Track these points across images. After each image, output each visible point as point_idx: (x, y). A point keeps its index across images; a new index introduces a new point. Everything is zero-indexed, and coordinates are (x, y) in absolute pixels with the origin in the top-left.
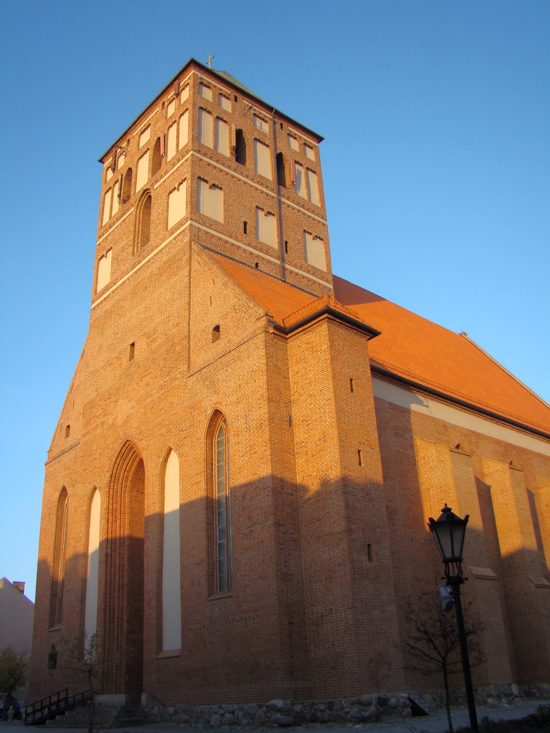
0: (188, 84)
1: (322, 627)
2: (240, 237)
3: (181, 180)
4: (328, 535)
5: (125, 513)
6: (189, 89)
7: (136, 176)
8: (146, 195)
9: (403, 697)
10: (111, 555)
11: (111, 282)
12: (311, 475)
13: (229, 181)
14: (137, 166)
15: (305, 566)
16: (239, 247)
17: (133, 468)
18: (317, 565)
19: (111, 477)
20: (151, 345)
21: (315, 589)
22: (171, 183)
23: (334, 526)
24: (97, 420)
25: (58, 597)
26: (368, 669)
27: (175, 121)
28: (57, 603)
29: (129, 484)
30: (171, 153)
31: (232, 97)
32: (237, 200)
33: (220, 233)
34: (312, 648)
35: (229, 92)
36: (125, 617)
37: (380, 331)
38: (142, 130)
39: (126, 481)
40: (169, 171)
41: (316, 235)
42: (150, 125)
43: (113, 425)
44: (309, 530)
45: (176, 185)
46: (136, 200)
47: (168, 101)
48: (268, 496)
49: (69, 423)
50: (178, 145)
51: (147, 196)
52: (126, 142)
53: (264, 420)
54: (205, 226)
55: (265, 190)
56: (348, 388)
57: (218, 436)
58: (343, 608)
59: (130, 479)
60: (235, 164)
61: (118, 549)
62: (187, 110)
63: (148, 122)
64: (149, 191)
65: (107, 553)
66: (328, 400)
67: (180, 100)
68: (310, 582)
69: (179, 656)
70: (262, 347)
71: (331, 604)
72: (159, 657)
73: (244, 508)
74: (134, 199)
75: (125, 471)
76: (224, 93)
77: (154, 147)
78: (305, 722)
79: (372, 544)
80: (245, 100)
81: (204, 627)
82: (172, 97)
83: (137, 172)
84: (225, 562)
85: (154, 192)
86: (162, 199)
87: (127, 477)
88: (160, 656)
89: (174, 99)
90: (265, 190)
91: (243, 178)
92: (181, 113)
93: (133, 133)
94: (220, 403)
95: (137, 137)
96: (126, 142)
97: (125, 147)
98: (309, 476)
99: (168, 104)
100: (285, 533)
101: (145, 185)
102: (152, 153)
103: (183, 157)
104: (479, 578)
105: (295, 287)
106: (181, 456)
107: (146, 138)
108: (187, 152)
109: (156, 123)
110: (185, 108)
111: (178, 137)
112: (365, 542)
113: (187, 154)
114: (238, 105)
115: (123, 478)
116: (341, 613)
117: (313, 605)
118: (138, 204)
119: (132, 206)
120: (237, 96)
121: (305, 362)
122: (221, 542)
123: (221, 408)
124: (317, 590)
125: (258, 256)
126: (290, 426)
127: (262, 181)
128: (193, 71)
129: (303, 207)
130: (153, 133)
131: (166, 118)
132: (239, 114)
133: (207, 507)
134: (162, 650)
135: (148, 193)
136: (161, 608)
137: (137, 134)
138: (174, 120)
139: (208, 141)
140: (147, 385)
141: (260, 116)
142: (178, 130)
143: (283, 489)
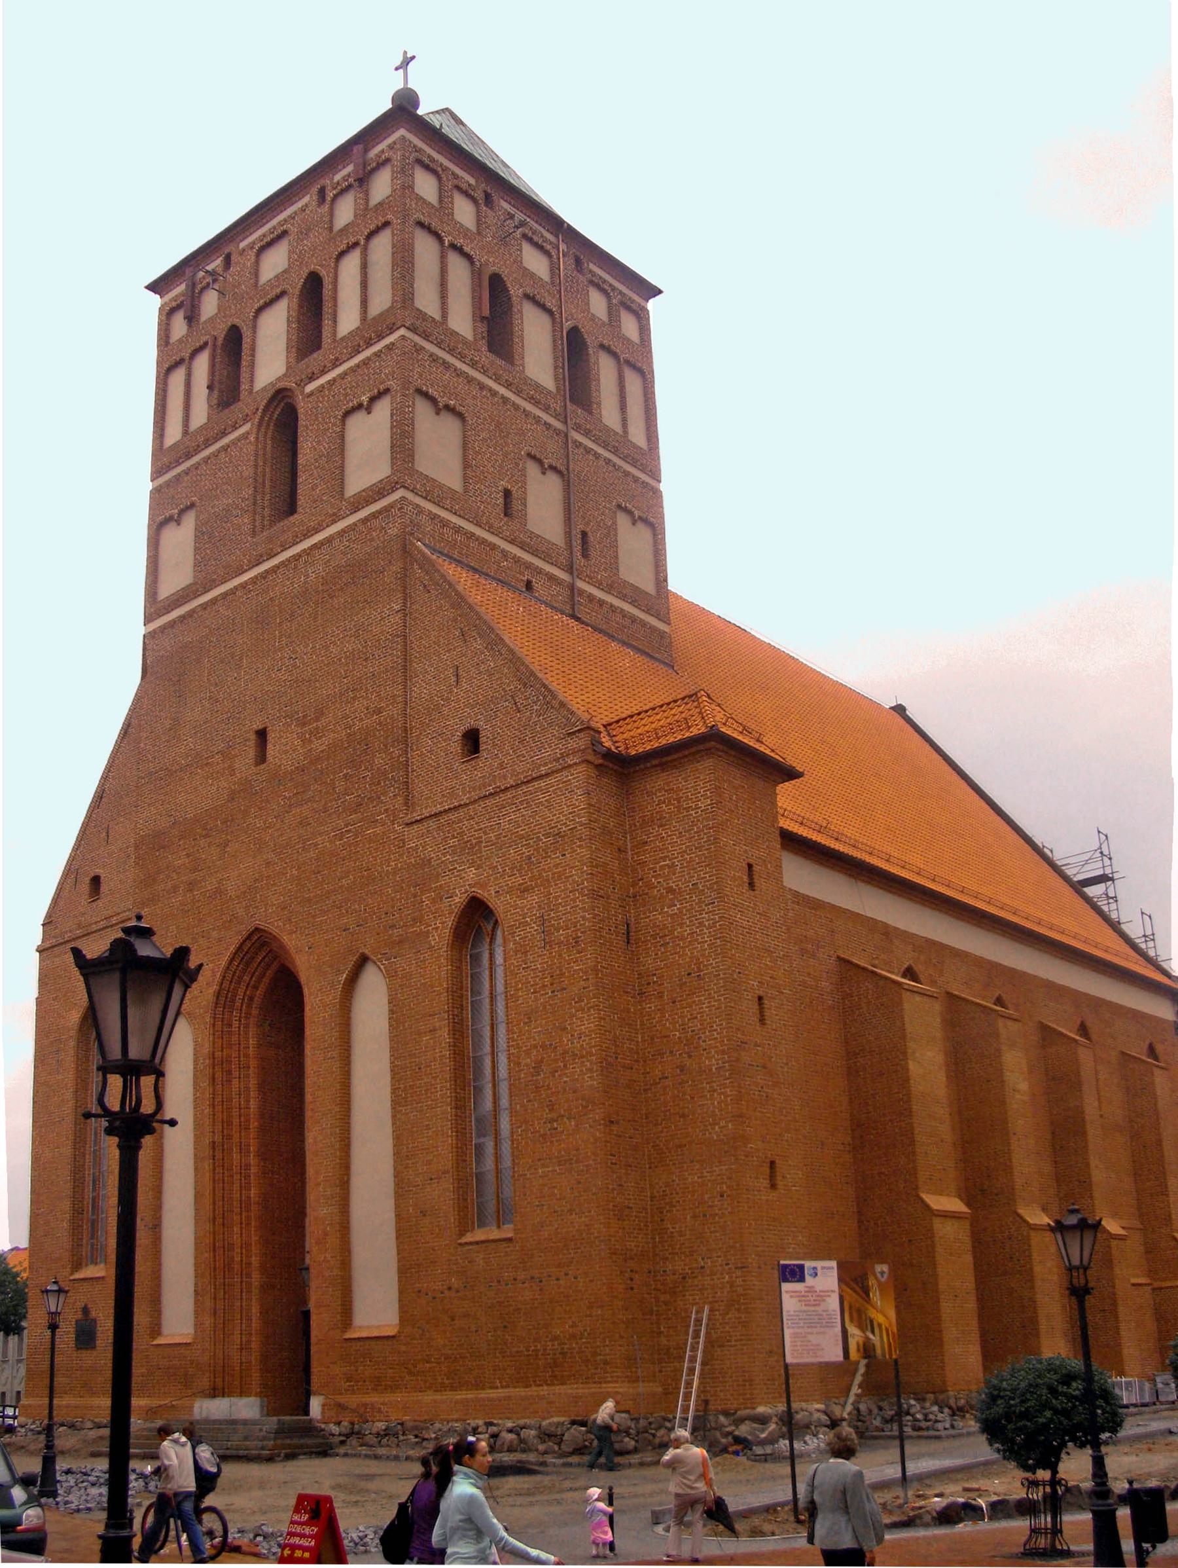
0: (388, 160)
1: (684, 1296)
2: (496, 524)
3: (376, 391)
4: (701, 1143)
5: (249, 1067)
6: (392, 176)
7: (253, 349)
8: (280, 402)
9: (818, 1411)
10: (223, 1146)
11: (195, 584)
12: (669, 1036)
13: (474, 397)
14: (254, 328)
15: (652, 1193)
16: (493, 547)
17: (266, 980)
18: (677, 1194)
19: (218, 997)
20: (310, 741)
21: (672, 1233)
22: (348, 390)
23: (714, 1129)
24: (175, 876)
25: (85, 1215)
26: (766, 1366)
27: (356, 244)
28: (85, 1227)
29: (255, 1012)
30: (348, 320)
31: (479, 195)
32: (491, 441)
33: (460, 516)
34: (662, 1329)
35: (472, 181)
36: (255, 1260)
37: (801, 770)
38: (265, 241)
39: (249, 1006)
40: (344, 361)
41: (641, 514)
42: (285, 233)
43: (219, 892)
44: (662, 1132)
45: (365, 399)
46: (257, 409)
47: (335, 189)
48: (591, 1070)
49: (99, 871)
50: (364, 303)
51: (283, 404)
52: (221, 258)
53: (582, 933)
54: (430, 500)
55: (545, 417)
56: (744, 882)
57: (472, 945)
58: (727, 1267)
59: (257, 1001)
60: (486, 357)
61: (236, 1136)
62: (387, 224)
63: (280, 224)
64: (289, 394)
65: (214, 1142)
66: (709, 904)
67: (367, 193)
68: (662, 1220)
69: (393, 1337)
70: (579, 792)
71: (703, 1259)
72: (347, 1336)
73: (537, 1088)
74: (245, 405)
75: (247, 987)
76: (464, 186)
77: (301, 291)
78: (650, 1448)
79: (777, 1161)
80: (506, 201)
81: (450, 1289)
82: (345, 179)
83: (254, 341)
84: (491, 1178)
85: (303, 399)
86: (326, 423)
87: (251, 999)
88: (349, 1335)
89: (350, 186)
90: (545, 417)
91: (502, 391)
92: (372, 227)
93: (241, 241)
94: (483, 886)
95: (252, 255)
96: (221, 258)
97: (220, 270)
98: (665, 1037)
99: (336, 197)
100: (620, 1136)
101: (279, 379)
102: (295, 306)
103: (381, 337)
104: (954, 1217)
105: (601, 631)
106: (390, 975)
107: (275, 262)
108: (392, 329)
109: (305, 232)
110: (382, 220)
111: (364, 285)
112: (766, 1157)
113: (391, 333)
114: (491, 217)
115: (243, 999)
116: (722, 1274)
117: (667, 1259)
118: (262, 418)
119: (245, 421)
120: (489, 191)
121: (661, 826)
122: (482, 1140)
123: (486, 895)
124: (675, 1234)
125: (529, 566)
126: (628, 943)
127: (535, 394)
128: (401, 132)
129: (615, 451)
130: (296, 258)
131: (331, 229)
132: (494, 237)
133: (455, 1077)
134: (351, 1324)
135: (284, 397)
136: (349, 1251)
137: (251, 247)
138: (352, 240)
139: (427, 301)
140: (303, 823)
141: (535, 238)
142: (364, 266)
143: (617, 1058)
